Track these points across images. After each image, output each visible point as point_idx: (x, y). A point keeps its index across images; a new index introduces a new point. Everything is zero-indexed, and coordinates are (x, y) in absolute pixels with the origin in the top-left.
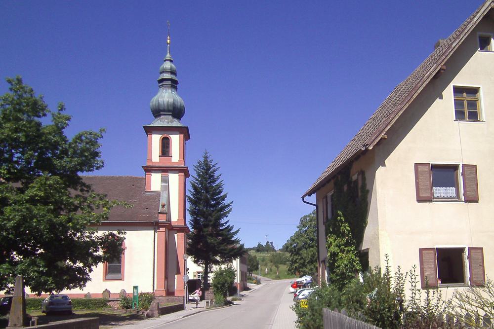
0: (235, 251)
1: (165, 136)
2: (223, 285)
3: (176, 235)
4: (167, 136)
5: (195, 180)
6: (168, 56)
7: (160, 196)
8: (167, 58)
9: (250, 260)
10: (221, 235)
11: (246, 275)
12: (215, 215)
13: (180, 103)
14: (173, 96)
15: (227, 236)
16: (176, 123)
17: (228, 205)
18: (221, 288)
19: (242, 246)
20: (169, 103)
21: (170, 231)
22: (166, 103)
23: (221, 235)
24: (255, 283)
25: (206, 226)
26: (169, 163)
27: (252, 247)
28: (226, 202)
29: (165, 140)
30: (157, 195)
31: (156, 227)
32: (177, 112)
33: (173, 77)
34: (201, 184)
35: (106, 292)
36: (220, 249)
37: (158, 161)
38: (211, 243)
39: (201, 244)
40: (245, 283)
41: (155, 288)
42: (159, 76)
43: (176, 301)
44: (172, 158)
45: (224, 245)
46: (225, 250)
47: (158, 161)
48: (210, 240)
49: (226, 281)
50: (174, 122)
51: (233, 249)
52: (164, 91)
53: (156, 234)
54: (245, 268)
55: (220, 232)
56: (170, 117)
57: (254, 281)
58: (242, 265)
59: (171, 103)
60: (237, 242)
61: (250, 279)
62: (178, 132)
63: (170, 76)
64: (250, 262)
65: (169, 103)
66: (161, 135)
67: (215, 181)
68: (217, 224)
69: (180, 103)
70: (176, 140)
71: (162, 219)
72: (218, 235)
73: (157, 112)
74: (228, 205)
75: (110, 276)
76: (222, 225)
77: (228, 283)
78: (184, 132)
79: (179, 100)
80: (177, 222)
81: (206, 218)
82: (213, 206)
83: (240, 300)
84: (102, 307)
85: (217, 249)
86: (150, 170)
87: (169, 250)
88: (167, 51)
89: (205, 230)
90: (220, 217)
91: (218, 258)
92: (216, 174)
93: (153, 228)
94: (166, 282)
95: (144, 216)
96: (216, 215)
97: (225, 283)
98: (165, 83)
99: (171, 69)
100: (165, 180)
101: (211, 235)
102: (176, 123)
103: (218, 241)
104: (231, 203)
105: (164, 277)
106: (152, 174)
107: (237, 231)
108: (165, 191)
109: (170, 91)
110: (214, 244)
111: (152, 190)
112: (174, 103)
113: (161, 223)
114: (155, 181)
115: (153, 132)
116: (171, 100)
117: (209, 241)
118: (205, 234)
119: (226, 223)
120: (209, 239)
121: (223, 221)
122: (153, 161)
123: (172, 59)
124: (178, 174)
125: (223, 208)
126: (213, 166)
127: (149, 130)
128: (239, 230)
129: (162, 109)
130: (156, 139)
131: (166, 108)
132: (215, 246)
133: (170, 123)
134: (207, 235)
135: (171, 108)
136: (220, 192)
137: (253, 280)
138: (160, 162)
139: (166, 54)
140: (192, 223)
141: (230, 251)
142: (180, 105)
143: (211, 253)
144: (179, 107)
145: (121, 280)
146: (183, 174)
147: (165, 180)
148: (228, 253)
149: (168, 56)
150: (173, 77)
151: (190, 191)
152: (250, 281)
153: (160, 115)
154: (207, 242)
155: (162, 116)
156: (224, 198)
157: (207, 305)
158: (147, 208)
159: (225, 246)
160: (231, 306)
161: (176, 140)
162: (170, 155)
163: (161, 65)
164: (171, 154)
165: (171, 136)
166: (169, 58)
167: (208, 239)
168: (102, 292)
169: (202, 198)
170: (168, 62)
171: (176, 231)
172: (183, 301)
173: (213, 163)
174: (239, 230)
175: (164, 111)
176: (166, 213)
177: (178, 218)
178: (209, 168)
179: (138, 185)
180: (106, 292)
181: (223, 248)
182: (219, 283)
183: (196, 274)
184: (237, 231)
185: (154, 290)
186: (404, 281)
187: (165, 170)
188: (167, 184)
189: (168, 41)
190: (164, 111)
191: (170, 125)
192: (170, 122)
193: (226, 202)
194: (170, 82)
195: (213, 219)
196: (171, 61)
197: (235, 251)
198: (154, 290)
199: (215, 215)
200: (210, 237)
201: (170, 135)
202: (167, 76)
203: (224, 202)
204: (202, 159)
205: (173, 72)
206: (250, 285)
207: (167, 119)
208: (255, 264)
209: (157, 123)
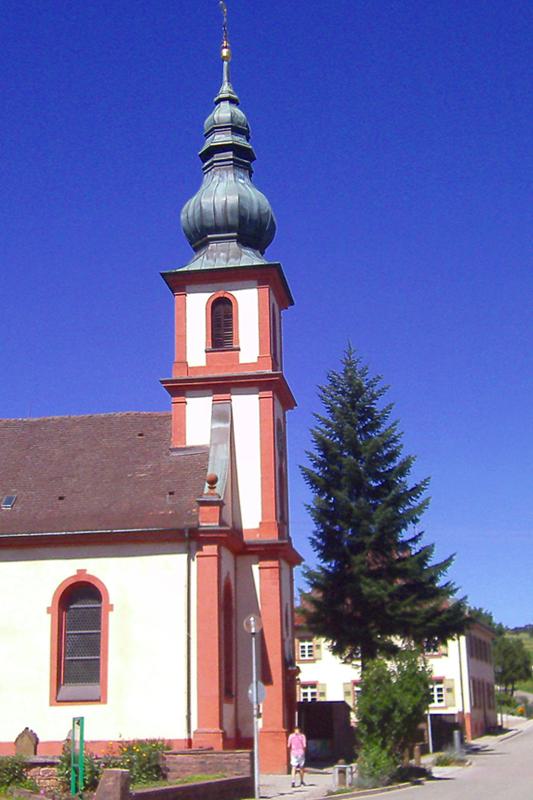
0: (444, 616)
1: (221, 294)
2: (387, 715)
3: (255, 568)
4: (226, 296)
5: (323, 427)
6: (226, 89)
7: (207, 460)
8: (221, 96)
9: (505, 651)
10: (403, 573)
11: (491, 692)
12: (381, 514)
13: (259, 203)
14: (239, 189)
15: (420, 582)
16: (249, 259)
17: (416, 490)
18: (381, 724)
19: (459, 605)
20: (229, 207)
21: (239, 558)
22: (219, 208)
23: (403, 573)
24: (521, 715)
25: (358, 548)
26: (233, 366)
27: (523, 626)
28: (410, 481)
29: (221, 308)
30: (201, 455)
31: (194, 544)
32: (250, 230)
33: (241, 141)
34: (340, 434)
35: (26, 738)
36: (399, 612)
37: (203, 363)
38: (371, 595)
39: (349, 601)
40: (490, 713)
41: (194, 726)
42: (203, 143)
43: (229, 767)
44: (241, 353)
45: (407, 601)
46: (413, 615)
47: (203, 363)
48: (370, 588)
49: (395, 704)
50: (244, 257)
51: (436, 613)
52: (216, 178)
53: (194, 565)
54: (488, 673)
55: (398, 566)
56: (234, 245)
57: (520, 708)
58: (474, 660)
59: (232, 205)
60: (448, 590)
61: (508, 703)
62: (255, 282)
63: (229, 138)
64: (506, 657)
65: (229, 207)
66: (210, 295)
67: (378, 425)
68: (386, 541)
69: (259, 203)
70: (248, 302)
71: (208, 521)
72: (391, 572)
73: (200, 236)
74: (416, 490)
75: (68, 690)
76: (404, 546)
77: (402, 711)
78: (267, 277)
79: (254, 197)
80: (257, 530)
81: (356, 526)
82: (375, 494)
83: (461, 762)
84: (8, 784)
85: (389, 612)
86: (183, 388)
87: (229, 605)
88: (222, 79)
89: (357, 558)
90: (399, 523)
91: (397, 641)
92: (378, 406)
93: (184, 546)
94: (229, 709)
95: (163, 511)
96: (382, 517)
97: (392, 711)
98: (217, 157)
99: (232, 121)
100: (223, 415)
101: (375, 575)
102: (249, 259)
103: (391, 589)
104: (424, 483)
105: (216, 691)
106: (188, 400)
107: (447, 563)
108: (221, 443)
109: (231, 177)
110: (380, 598)
111: (189, 443)
112: (240, 207)
113: (204, 532)
114: (197, 418)
115: (188, 288)
116: (233, 200)
117: (366, 590)
118: (356, 570)
119: (414, 540)
120: (365, 584)
121: (405, 535)
122: (190, 365)
123: (235, 96)
124: (257, 396)
125: (398, 501)
126: (370, 385)
127: (181, 282)
128: (451, 559)
129: (209, 224)
130: (196, 306)
131: (221, 222)
132: (383, 604)
133: (231, 260)
134: (362, 572)
135: (233, 221)
136: (391, 457)
137: (515, 707)
138: (208, 367)
139: (221, 84)
140: (319, 541)
141: (429, 620)
142: (259, 210)
143: (372, 625)
144: (255, 218)
145: (97, 701)
146: (269, 393)
147: (223, 415)
148: (422, 625)
149: (226, 89)
150: (241, 141)
151: (312, 456)
152: (508, 709)
153: (206, 244)
154: (362, 594)
155: (212, 246)
156: (403, 470)
157: (342, 782)
158: (171, 493)
159: (414, 603)
160: (419, 783)
161: (248, 302)
162: (235, 346)
163: (205, 118)
164: (238, 343)
165: (235, 293)
166: (227, 95)
167: (362, 585)
168: (14, 740)
169: (344, 471)
170: (225, 105)
171: (256, 557)
172: (248, 768)
173: (370, 377)
174: (451, 559)
175: (217, 229)
176: (221, 504)
177: (260, 520)
178: (359, 392)
179: (155, 433)
180: (26, 738)
181: (408, 609)
182: (372, 710)
183: (350, 688)
184: (447, 563)
185: (189, 732)
186: (17, 764)
187: (221, 386)
188: (228, 425)
189: (225, 52)
190: (217, 229)
191: (233, 263)
192: (233, 257)
193: (410, 481)
194: (230, 155)
195: (373, 528)
196: (232, 101)
197: (444, 616)
198: (189, 732)
199: (381, 514)
200: (368, 581)
201: (232, 293)
202: (221, 138)
203: (403, 479)
204: (339, 369)
205: (236, 130)
206: (504, 718)
207: (223, 251)
208: (519, 662)
209: (200, 263)
